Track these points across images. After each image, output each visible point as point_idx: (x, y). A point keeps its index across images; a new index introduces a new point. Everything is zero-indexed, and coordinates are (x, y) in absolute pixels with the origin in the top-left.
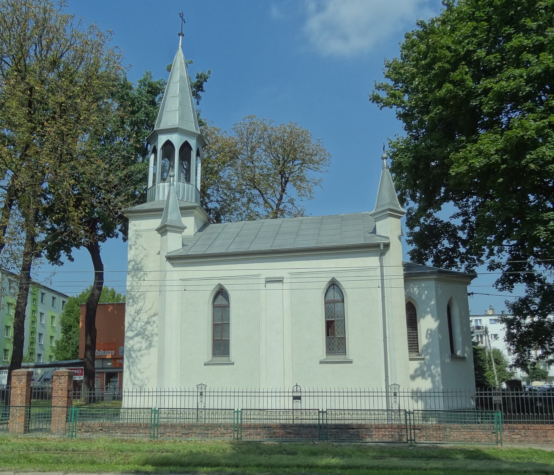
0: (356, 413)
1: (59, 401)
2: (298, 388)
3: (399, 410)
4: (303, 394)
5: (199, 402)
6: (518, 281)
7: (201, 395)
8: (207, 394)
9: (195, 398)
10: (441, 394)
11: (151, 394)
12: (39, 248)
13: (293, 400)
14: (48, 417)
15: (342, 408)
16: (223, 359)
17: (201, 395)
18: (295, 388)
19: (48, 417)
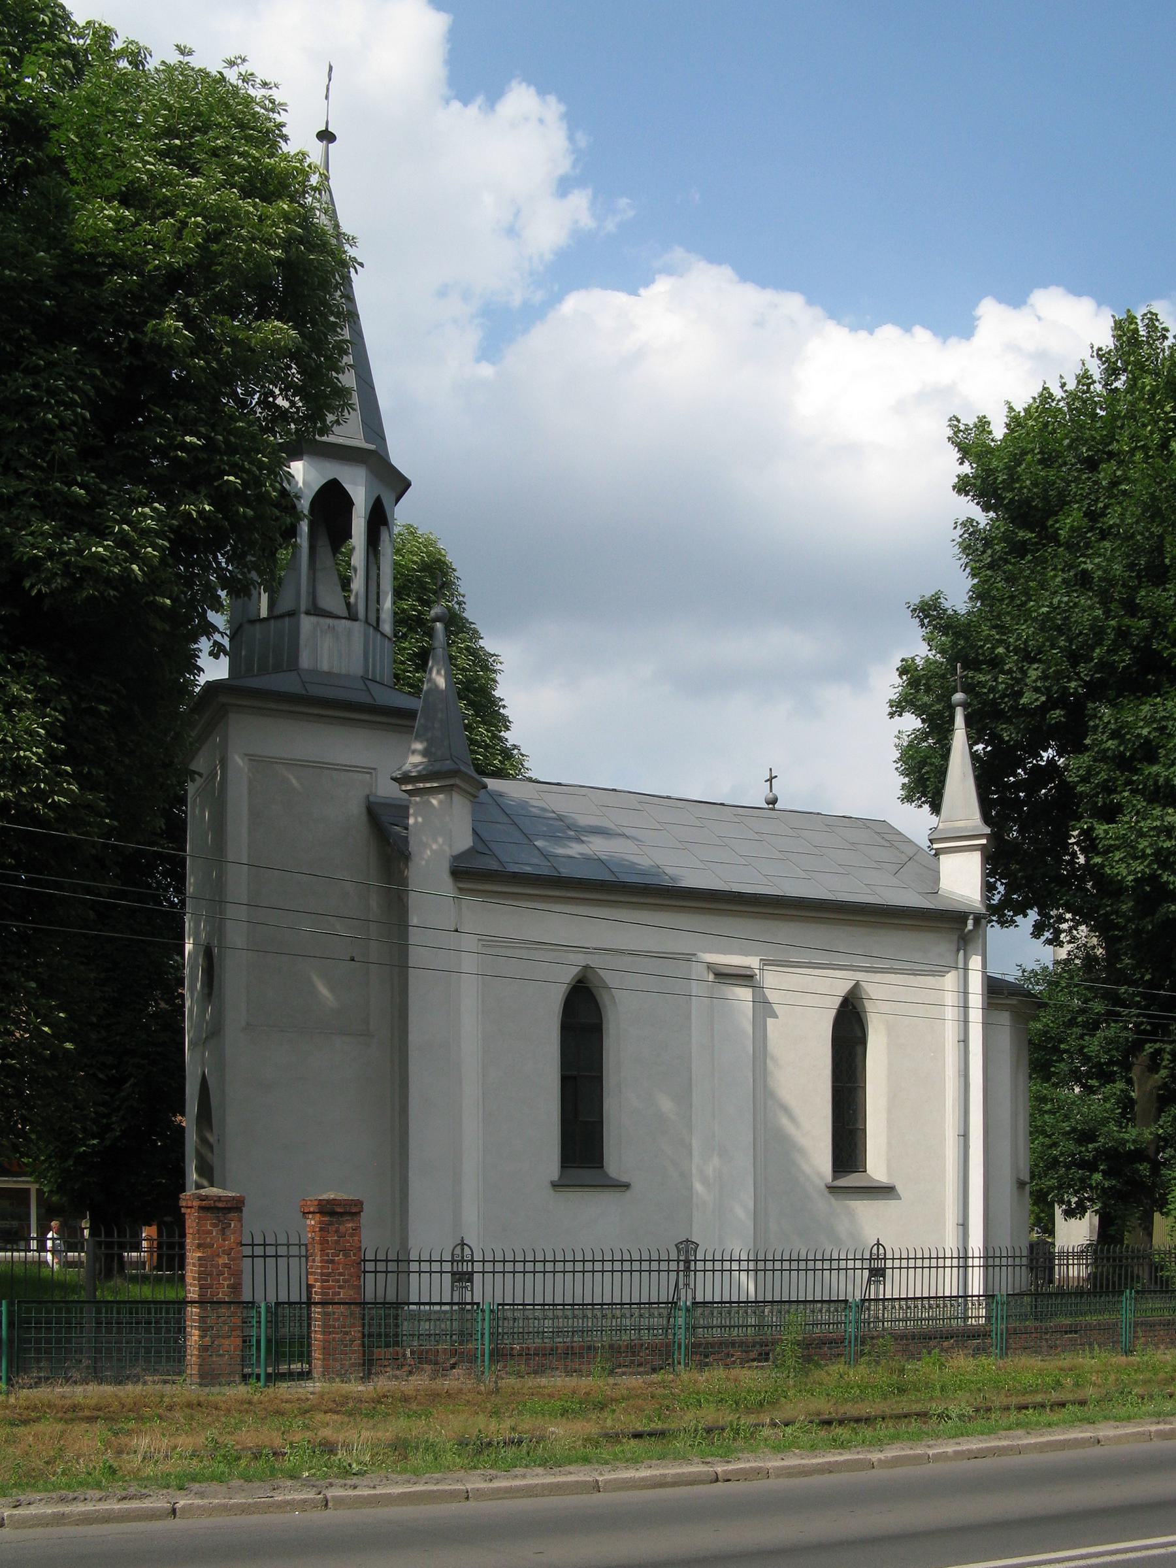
0: (550, 1314)
1: (340, 1287)
2: (467, 1251)
3: (965, 1297)
4: (478, 1267)
5: (681, 1285)
6: (570, 838)
7: (687, 1269)
8: (700, 1266)
9: (673, 1275)
10: (414, 1266)
11: (519, 1267)
12: (283, 501)
13: (453, 1283)
14: (1036, 1306)
15: (918, 1295)
16: (587, 1175)
17: (687, 1269)
18: (458, 1251)
19: (1036, 1306)
